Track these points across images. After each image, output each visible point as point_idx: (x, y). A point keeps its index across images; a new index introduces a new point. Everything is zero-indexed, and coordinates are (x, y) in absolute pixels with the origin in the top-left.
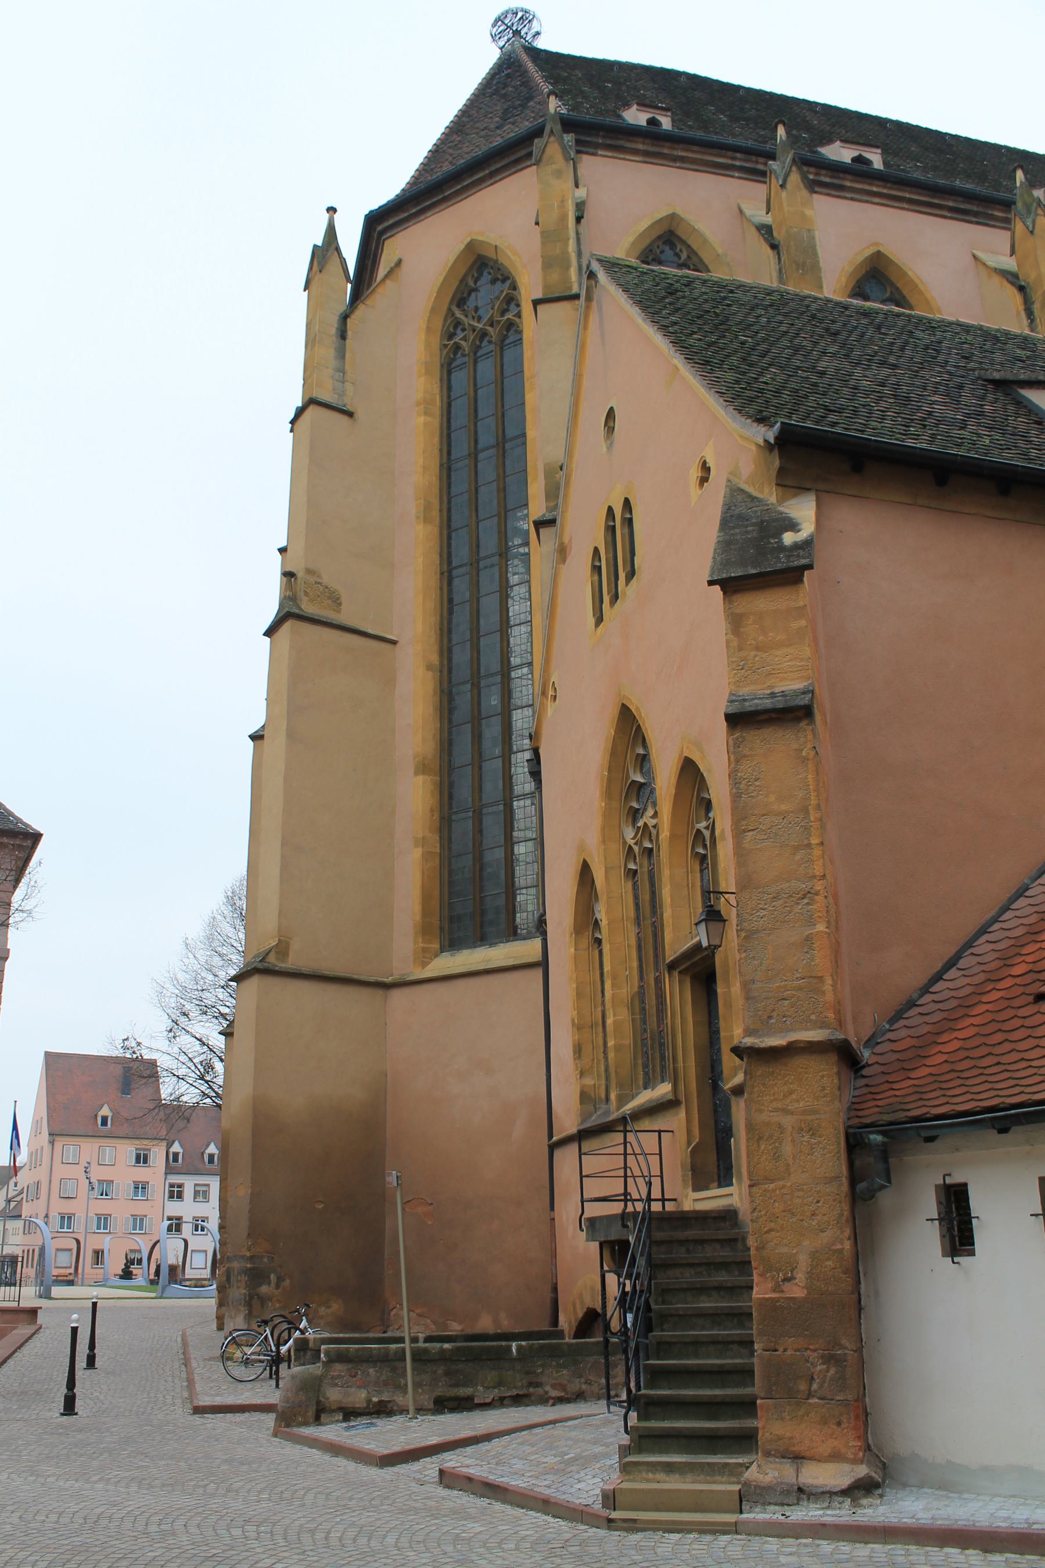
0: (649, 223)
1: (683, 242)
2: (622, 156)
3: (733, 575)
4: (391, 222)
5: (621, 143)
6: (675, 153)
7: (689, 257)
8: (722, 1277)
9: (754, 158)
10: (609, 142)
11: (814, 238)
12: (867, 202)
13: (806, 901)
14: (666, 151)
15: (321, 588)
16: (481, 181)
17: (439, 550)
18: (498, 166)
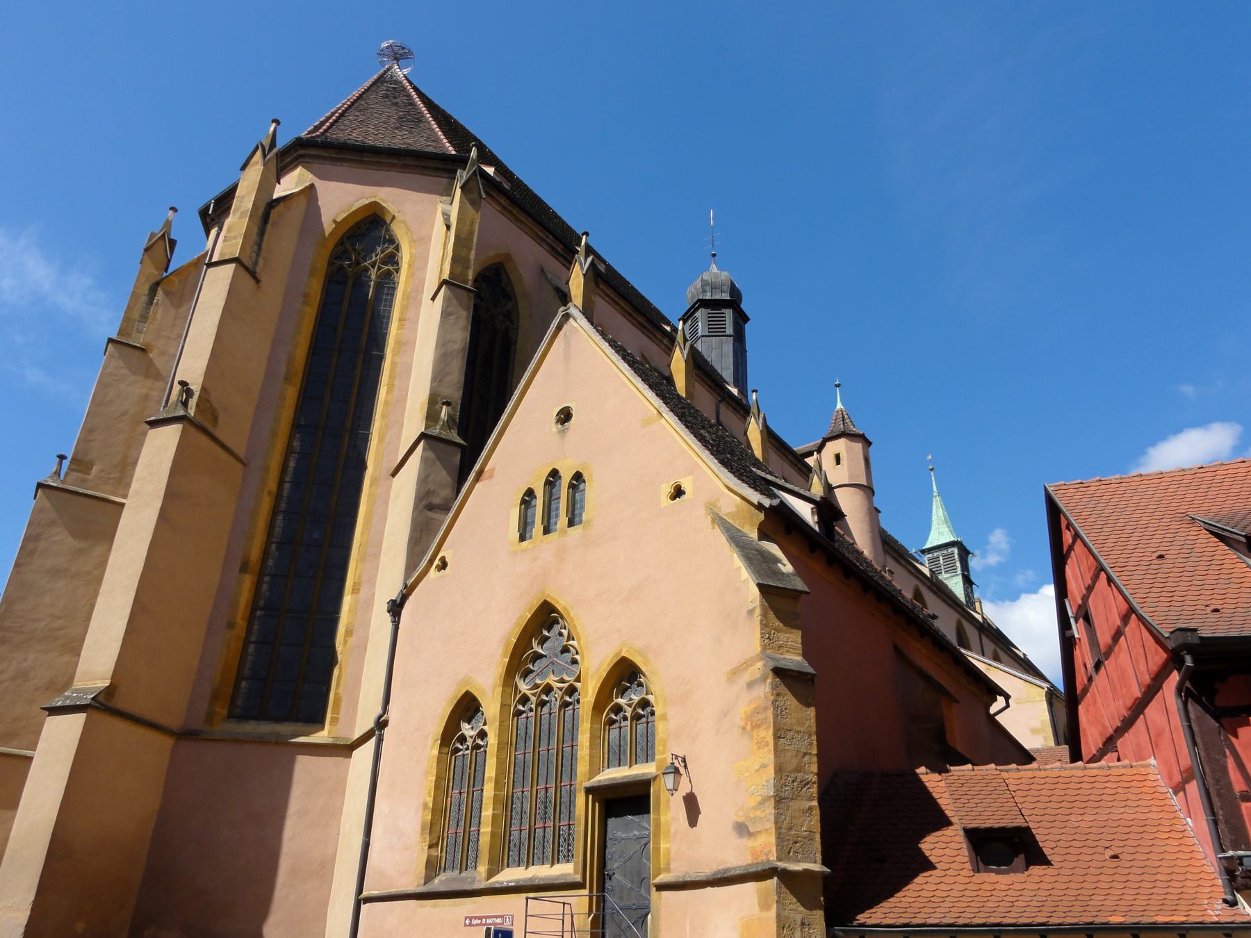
1: (507, 274)
5: (493, 194)
9: (557, 242)
14: (515, 212)
15: (208, 405)
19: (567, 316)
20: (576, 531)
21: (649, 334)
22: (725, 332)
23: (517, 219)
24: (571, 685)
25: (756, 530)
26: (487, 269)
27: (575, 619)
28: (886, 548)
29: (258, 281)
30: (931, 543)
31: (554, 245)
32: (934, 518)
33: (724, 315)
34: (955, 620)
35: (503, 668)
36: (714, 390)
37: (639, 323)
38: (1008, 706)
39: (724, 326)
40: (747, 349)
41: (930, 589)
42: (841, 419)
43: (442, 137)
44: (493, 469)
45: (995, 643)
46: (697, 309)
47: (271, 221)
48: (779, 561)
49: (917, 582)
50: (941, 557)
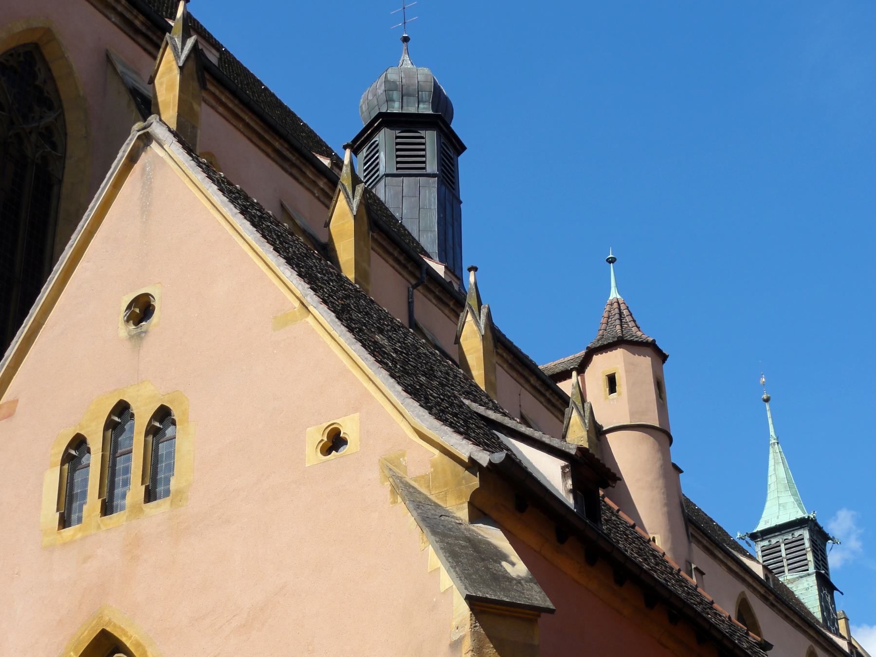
3: (488, 596)
8: (789, 545)
9: (135, 12)
11: (195, 136)
12: (212, 107)
19: (146, 139)
20: (159, 508)
22: (424, 168)
25: (466, 505)
28: (691, 530)
30: (766, 522)
31: (128, 15)
32: (771, 480)
36: (405, 267)
39: (423, 159)
40: (462, 198)
41: (765, 599)
42: (617, 316)
44: (15, 402)
46: (377, 130)
48: (505, 557)
49: (742, 588)
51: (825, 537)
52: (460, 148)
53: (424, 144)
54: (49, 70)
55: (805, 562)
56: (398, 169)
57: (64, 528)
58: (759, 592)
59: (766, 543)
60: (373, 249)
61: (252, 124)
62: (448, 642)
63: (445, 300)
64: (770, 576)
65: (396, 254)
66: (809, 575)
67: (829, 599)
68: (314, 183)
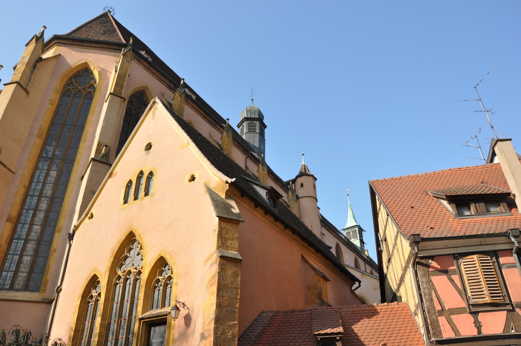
0: (140, 86)
1: (146, 95)
2: (140, 64)
3: (224, 216)
4: (61, 41)
5: (141, 61)
6: (153, 71)
7: (146, 100)
9: (171, 83)
10: (138, 58)
12: (192, 108)
13: (234, 313)
14: (151, 69)
16: (97, 47)
17: (40, 149)
18: (104, 46)
19: (154, 102)
20: (147, 198)
21: (214, 126)
22: (256, 131)
23: (152, 72)
24: (140, 270)
25: (225, 194)
26: (137, 92)
27: (143, 239)
28: (322, 223)
29: (28, 93)
30: (347, 226)
31: (169, 84)
32: (349, 215)
33: (255, 124)
34: (355, 256)
35: (110, 263)
36: (244, 152)
37: (209, 121)
38: (360, 286)
39: (255, 129)
40: (265, 139)
41: (343, 244)
42: (304, 169)
43: (122, 38)
44: (117, 172)
45: (371, 267)
46: (244, 122)
47: (37, 67)
48: (233, 208)
49: (337, 240)
50: (351, 232)
51: (362, 230)
52: (265, 127)
53: (472, 292)
54: (147, 97)
55: (357, 236)
56: (249, 131)
57: (125, 204)
58: (342, 242)
59: (347, 231)
60: (233, 145)
61: (202, 113)
62: (213, 230)
63: (256, 161)
64: (346, 238)
65: (242, 149)
66: (358, 239)
67: (363, 245)
68: (219, 129)
